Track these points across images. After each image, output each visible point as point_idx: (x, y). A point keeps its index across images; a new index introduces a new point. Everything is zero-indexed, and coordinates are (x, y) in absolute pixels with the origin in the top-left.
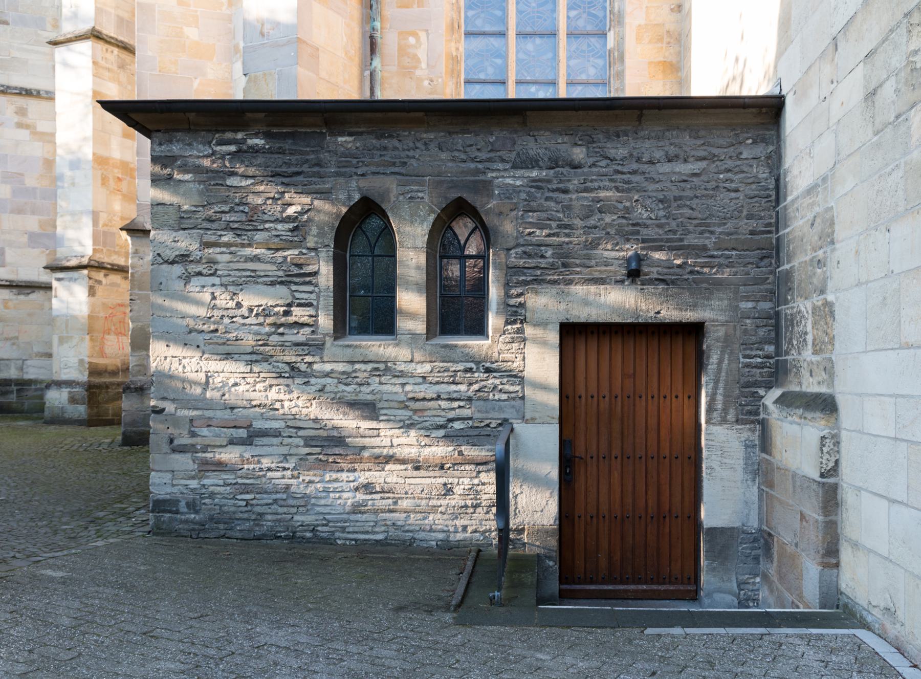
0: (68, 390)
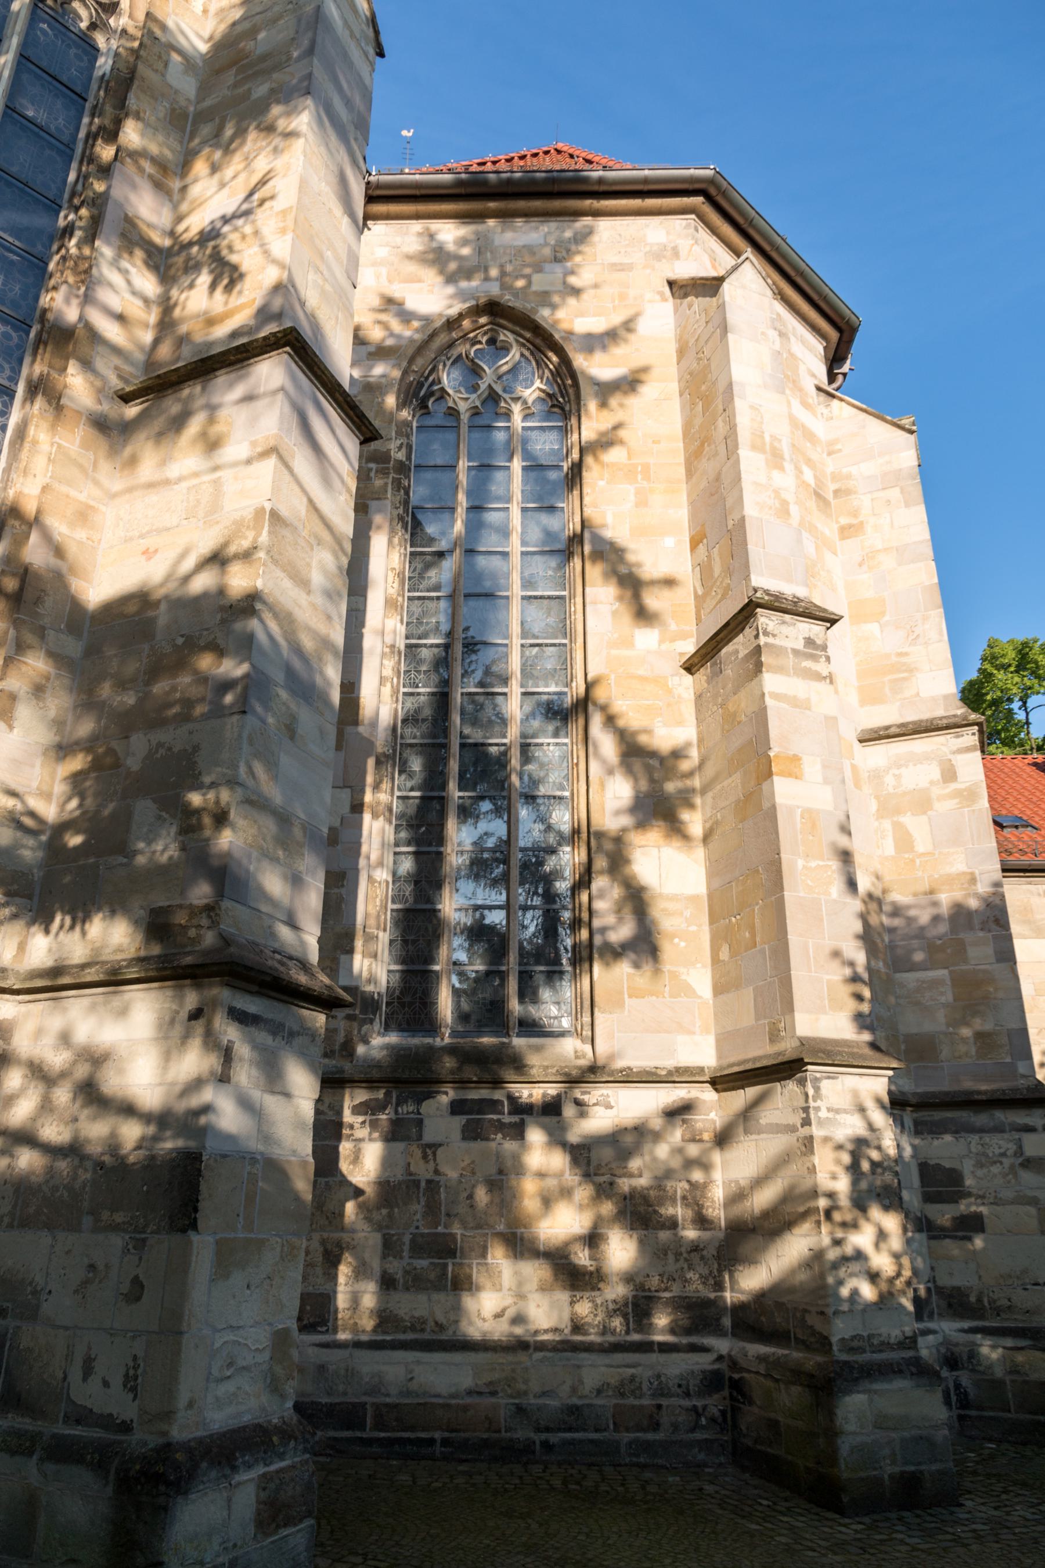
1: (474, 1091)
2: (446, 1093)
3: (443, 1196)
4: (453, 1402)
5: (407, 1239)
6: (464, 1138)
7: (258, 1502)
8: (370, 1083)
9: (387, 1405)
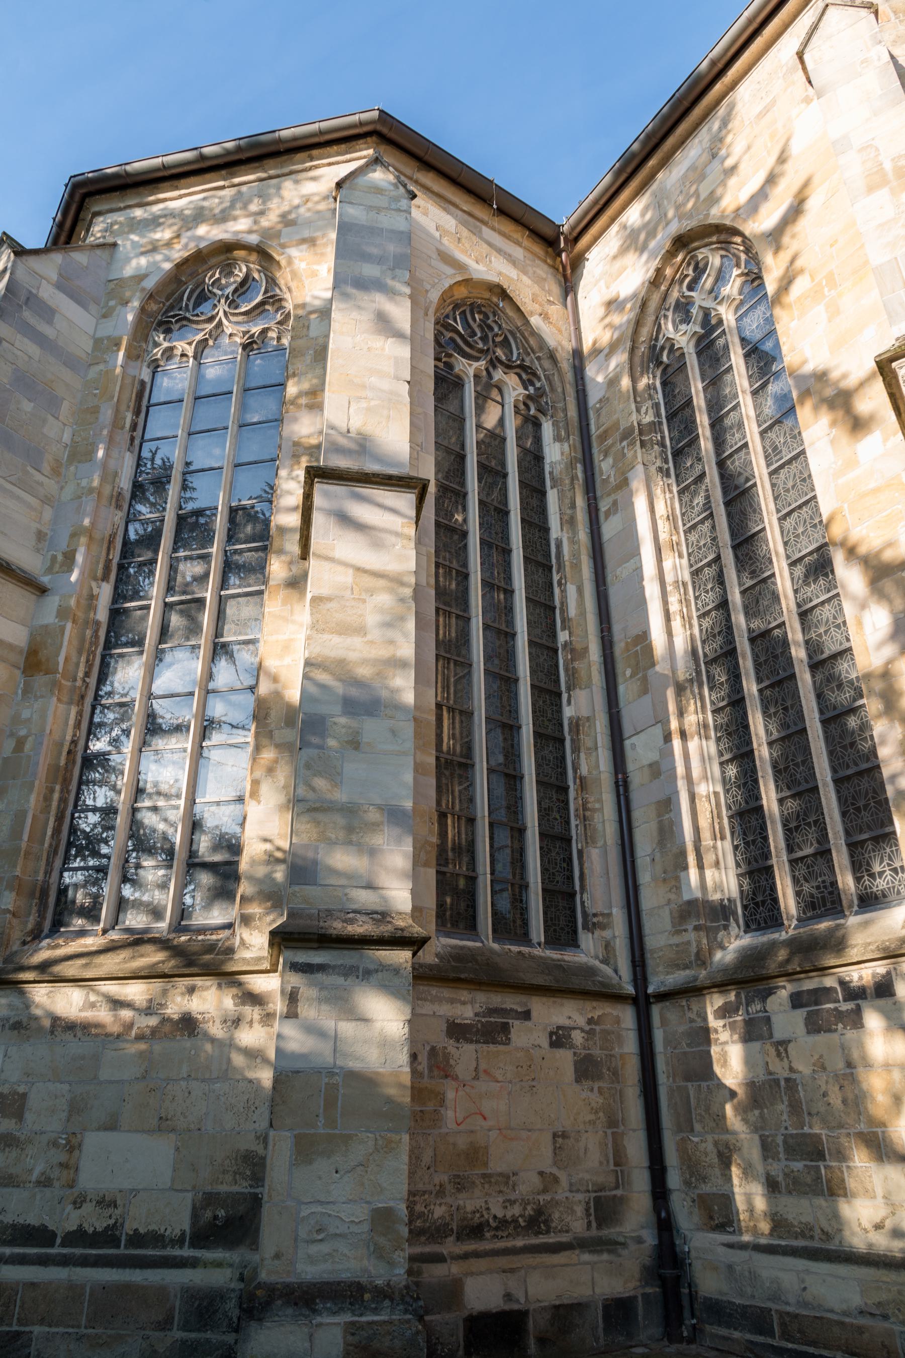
0: (348, 1317)
1: (807, 981)
2: (784, 987)
3: (802, 1094)
4: (847, 1320)
5: (780, 1140)
6: (808, 1032)
7: (347, 1344)
8: (721, 986)
9: (788, 1313)
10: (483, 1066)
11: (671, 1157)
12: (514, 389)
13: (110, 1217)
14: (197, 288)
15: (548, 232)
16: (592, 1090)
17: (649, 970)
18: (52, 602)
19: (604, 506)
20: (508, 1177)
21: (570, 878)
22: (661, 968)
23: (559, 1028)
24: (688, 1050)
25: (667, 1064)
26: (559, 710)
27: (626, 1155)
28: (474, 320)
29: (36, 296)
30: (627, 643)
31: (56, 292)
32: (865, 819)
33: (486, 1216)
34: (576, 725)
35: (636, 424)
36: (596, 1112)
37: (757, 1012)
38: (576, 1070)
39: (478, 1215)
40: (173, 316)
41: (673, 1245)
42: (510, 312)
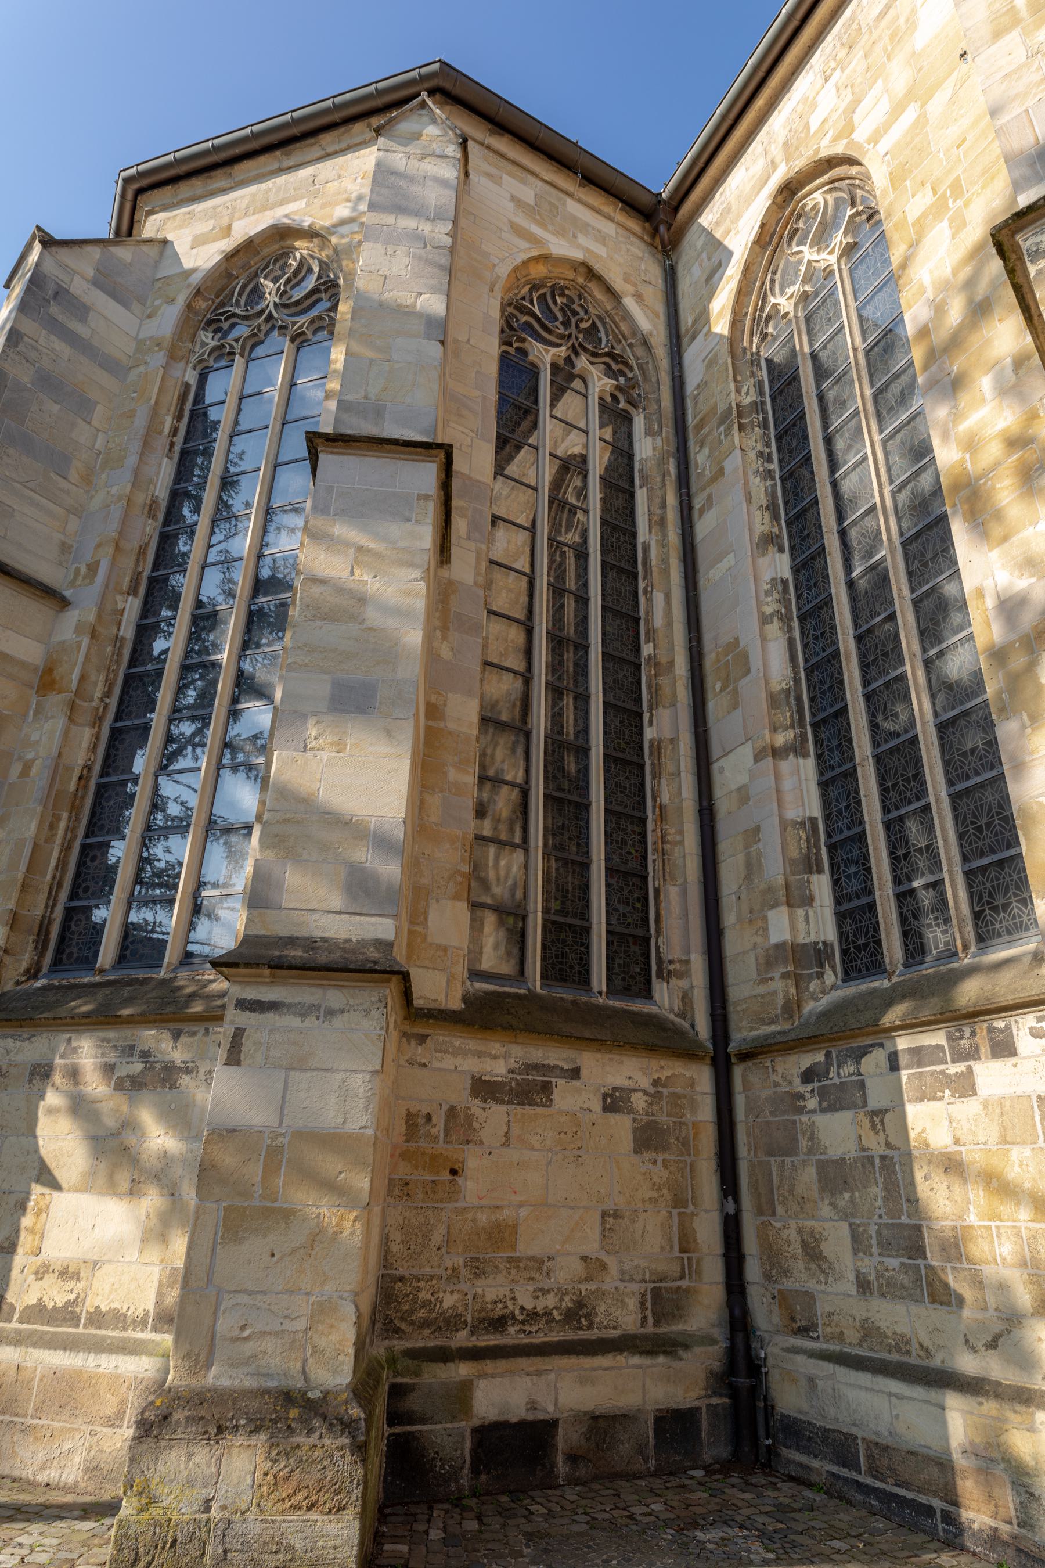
5: (873, 1230)
10: (515, 1131)
11: (751, 1245)
12: (600, 379)
13: (72, 1291)
14: (249, 282)
15: (645, 200)
16: (655, 1162)
17: (732, 1025)
18: (72, 617)
19: (698, 503)
20: (542, 1262)
21: (646, 920)
22: (744, 1023)
23: (615, 1089)
24: (771, 1119)
25: (748, 1135)
26: (640, 733)
27: (695, 1240)
28: (555, 303)
29: (67, 291)
30: (718, 654)
31: (93, 288)
32: (987, 841)
33: (511, 1307)
34: (657, 747)
35: (734, 406)
36: (659, 1189)
37: (850, 1075)
38: (635, 1140)
39: (500, 1306)
40: (222, 314)
41: (748, 1348)
42: (599, 294)
